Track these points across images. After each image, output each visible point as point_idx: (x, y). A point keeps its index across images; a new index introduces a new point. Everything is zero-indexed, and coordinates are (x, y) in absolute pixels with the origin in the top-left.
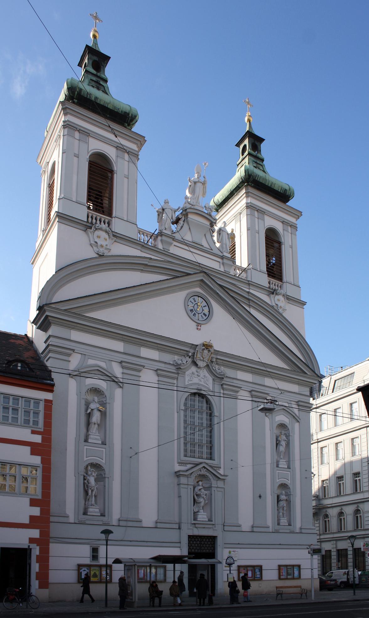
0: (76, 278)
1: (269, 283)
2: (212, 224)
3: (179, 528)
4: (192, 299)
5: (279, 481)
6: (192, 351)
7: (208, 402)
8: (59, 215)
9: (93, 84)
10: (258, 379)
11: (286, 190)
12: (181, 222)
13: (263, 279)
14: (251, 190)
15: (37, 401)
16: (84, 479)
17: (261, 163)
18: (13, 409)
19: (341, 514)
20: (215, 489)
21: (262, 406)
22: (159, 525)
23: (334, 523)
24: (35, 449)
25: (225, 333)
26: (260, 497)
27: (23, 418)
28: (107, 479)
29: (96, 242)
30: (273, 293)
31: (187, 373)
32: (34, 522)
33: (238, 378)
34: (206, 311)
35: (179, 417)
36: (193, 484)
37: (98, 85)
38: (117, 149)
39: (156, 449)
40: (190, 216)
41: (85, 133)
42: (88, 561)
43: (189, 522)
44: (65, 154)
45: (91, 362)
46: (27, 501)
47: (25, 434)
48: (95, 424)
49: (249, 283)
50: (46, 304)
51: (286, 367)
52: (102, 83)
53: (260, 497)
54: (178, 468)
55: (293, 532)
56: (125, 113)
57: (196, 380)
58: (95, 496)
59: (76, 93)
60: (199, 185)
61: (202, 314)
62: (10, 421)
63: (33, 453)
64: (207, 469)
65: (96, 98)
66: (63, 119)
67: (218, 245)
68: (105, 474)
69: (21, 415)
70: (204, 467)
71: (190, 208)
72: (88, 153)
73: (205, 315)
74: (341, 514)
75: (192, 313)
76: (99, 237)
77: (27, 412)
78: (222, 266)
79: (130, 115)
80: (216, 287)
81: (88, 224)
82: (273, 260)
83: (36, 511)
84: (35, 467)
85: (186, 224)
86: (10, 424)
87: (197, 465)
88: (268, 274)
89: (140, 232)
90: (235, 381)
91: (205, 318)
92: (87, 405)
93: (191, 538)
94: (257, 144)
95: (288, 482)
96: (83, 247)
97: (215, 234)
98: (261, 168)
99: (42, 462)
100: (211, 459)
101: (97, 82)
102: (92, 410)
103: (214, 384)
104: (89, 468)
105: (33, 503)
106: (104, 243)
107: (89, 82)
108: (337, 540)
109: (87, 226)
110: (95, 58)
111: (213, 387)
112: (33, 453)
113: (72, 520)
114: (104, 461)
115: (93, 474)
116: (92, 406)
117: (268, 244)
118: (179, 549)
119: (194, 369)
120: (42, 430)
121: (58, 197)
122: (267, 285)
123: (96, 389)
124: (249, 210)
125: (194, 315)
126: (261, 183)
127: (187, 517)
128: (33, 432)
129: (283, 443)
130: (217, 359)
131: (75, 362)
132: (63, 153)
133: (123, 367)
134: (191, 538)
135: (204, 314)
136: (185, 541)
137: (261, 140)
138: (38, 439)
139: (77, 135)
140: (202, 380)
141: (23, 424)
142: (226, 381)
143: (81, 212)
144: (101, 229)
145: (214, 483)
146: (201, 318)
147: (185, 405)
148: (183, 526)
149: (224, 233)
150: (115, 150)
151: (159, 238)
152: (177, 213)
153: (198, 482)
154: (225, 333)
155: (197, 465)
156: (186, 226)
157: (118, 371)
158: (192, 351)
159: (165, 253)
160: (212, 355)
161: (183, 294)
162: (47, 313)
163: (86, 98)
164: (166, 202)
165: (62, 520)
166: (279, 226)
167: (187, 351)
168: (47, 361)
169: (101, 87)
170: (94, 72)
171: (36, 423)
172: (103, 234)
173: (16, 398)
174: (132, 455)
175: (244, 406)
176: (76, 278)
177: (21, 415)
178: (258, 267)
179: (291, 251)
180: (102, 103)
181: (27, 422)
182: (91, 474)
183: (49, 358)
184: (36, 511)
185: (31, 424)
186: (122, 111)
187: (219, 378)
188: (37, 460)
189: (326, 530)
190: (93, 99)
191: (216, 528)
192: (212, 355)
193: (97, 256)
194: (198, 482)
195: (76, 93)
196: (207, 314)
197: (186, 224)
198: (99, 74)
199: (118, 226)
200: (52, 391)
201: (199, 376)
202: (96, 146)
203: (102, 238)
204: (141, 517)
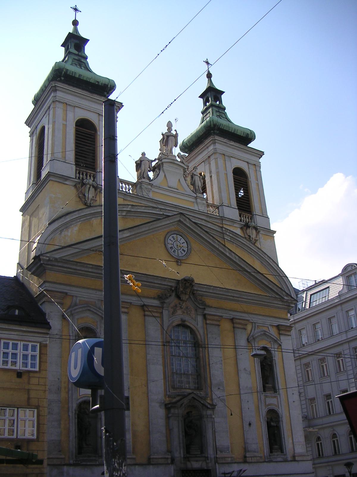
0: (31, 170)
1: (240, 216)
9: (76, 62)
11: (247, 134)
13: (233, 213)
17: (223, 112)
19: (334, 436)
21: (254, 353)
23: (328, 448)
37: (80, 63)
52: (83, 60)
56: (105, 84)
59: (63, 73)
61: (181, 250)
65: (80, 75)
70: (193, 397)
72: (74, 119)
73: (184, 251)
74: (334, 436)
79: (109, 86)
80: (187, 225)
82: (241, 193)
88: (238, 209)
91: (184, 253)
94: (219, 96)
98: (224, 116)
101: (79, 60)
107: (73, 61)
110: (77, 42)
117: (248, 206)
122: (238, 219)
126: (226, 131)
135: (183, 250)
152: (154, 164)
163: (72, 76)
164: (143, 154)
166: (244, 166)
168: (41, 304)
169: (82, 63)
170: (76, 52)
176: (31, 170)
180: (85, 79)
186: (102, 84)
189: (320, 455)
190: (77, 76)
195: (63, 73)
197: (161, 171)
198: (80, 54)
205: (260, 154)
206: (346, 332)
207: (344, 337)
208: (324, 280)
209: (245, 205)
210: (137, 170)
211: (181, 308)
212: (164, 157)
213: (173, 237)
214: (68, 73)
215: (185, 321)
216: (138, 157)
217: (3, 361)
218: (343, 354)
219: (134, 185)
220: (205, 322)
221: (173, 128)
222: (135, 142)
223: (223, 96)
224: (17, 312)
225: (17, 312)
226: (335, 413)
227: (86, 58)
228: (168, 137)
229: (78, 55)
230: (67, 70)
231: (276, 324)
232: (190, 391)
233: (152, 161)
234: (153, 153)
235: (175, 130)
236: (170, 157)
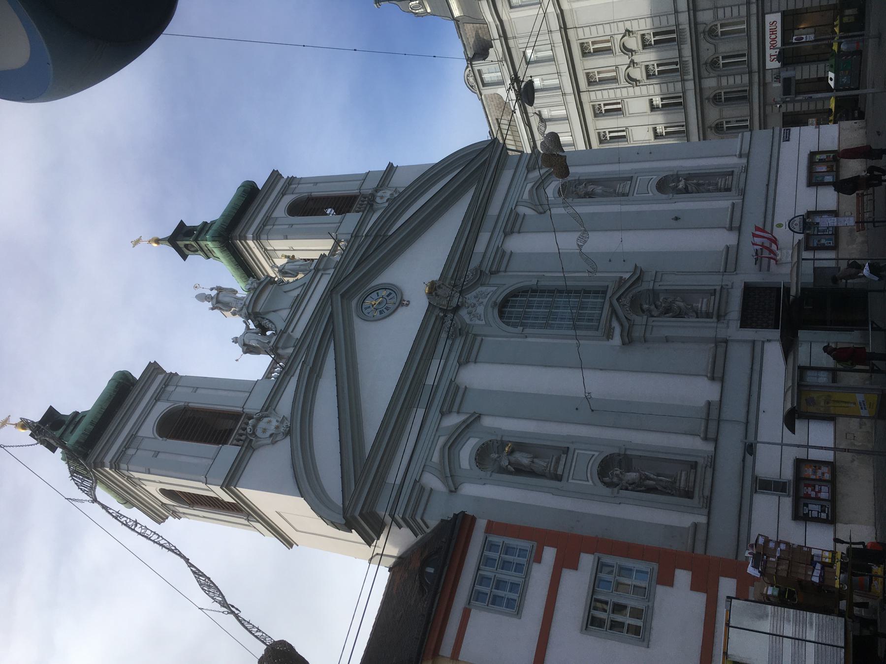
1: (358, 212)
2: (271, 281)
3: (726, 341)
4: (366, 312)
5: (653, 193)
6: (437, 312)
7: (514, 294)
8: (228, 484)
10: (488, 224)
12: (264, 322)
13: (352, 219)
14: (237, 232)
15: (488, 545)
16: (627, 489)
18: (497, 588)
20: (657, 284)
22: (718, 374)
24: (567, 561)
25: (418, 269)
26: (676, 219)
27: (513, 573)
28: (628, 452)
29: (271, 435)
30: (372, 205)
31: (468, 321)
32: (704, 583)
33: (483, 251)
34: (384, 293)
35: (534, 336)
36: (645, 317)
38: (159, 400)
39: (586, 372)
40: (258, 309)
41: (132, 438)
42: (787, 503)
43: (714, 325)
44: (152, 470)
45: (436, 458)
46: (661, 590)
47: (541, 574)
48: (533, 462)
49: (355, 235)
50: (344, 513)
51: (471, 192)
53: (676, 219)
54: (617, 340)
55: (746, 169)
57: (480, 310)
58: (658, 475)
60: (221, 298)
62: (515, 596)
63: (575, 566)
64: (622, 294)
65: (91, 423)
66: (108, 469)
67: (300, 276)
68: (619, 455)
69: (510, 576)
70: (618, 300)
71: (247, 309)
72: (155, 438)
73: (390, 294)
74: (716, 99)
75: (384, 313)
76: (264, 431)
77: (505, 565)
78: (328, 272)
80: (353, 282)
81: (246, 445)
83: (683, 577)
84: (600, 566)
85: (268, 317)
86: (522, 596)
87: (614, 312)
89: (268, 375)
90: (488, 255)
91: (393, 294)
92: (503, 470)
93: (745, 322)
95: (655, 178)
96: (276, 456)
97: (286, 279)
99: (591, 552)
100: (605, 292)
102: (510, 464)
103: (489, 285)
104: (607, 479)
105: (667, 580)
106: (274, 423)
108: (764, 103)
109: (249, 446)
111: (494, 285)
112: (575, 566)
113: (703, 520)
114: (596, 454)
115: (618, 472)
116: (505, 463)
118: (766, 345)
119: (463, 313)
120: (535, 544)
121: (203, 486)
123: (477, 454)
124: (262, 237)
125: (387, 309)
127: (708, 329)
128: (538, 559)
129: (590, 188)
130: (452, 278)
131: (432, 481)
132: (149, 473)
133: (450, 412)
134: (745, 322)
136: (750, 334)
137: (182, 224)
138: (549, 554)
139: (131, 452)
140: (481, 300)
141: (523, 575)
142: (486, 267)
143: (229, 452)
144: (254, 427)
145: (646, 285)
146: (396, 300)
147: (515, 325)
148: (722, 334)
149: (286, 267)
150: (159, 403)
151: (280, 351)
152: (252, 326)
153: (643, 311)
154: (418, 269)
155: (614, 312)
156: (271, 316)
157: (453, 420)
158: (437, 312)
159: (299, 344)
160: (447, 283)
161: (359, 325)
162: (357, 514)
164: (235, 340)
165: (701, 536)
166: (288, 199)
167: (436, 319)
168: (428, 527)
171: (522, 552)
172: (262, 424)
173: (480, 579)
174: (592, 409)
175: (518, 244)
177: (510, 576)
178: (335, 225)
179: (321, 185)
180: (99, 416)
181: (519, 568)
182: (617, 475)
183: (422, 519)
184: (683, 577)
185: (523, 561)
186: (115, 391)
187: (481, 277)
188: (587, 561)
190: (92, 427)
191: (730, 284)
192: (447, 283)
193: (288, 438)
194: (643, 311)
196: (389, 291)
197: (268, 317)
199: (255, 405)
200: (473, 519)
201: (474, 305)
202: (149, 429)
203: (270, 424)
204: (702, 403)
205: (275, 176)
206: (564, 94)
207: (571, 99)
208: (467, 82)
209: (343, 204)
210: (259, 353)
211: (474, 305)
212: (245, 310)
213: (366, 309)
214: (82, 441)
215: (495, 303)
216: (238, 349)
217: (507, 607)
218: (811, 648)
219: (275, 362)
220: (503, 274)
221: (208, 292)
222: (216, 354)
223: (188, 223)
224: (430, 570)
225: (430, 570)
226: (684, 129)
227: (76, 414)
228: (218, 302)
229: (68, 427)
230: (77, 442)
231: (524, 170)
232: (607, 306)
233: (248, 327)
234: (237, 325)
235: (212, 289)
236: (247, 303)
